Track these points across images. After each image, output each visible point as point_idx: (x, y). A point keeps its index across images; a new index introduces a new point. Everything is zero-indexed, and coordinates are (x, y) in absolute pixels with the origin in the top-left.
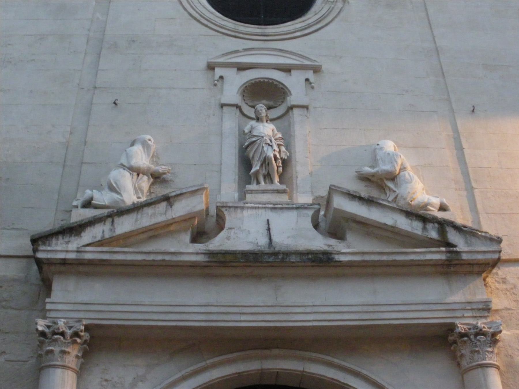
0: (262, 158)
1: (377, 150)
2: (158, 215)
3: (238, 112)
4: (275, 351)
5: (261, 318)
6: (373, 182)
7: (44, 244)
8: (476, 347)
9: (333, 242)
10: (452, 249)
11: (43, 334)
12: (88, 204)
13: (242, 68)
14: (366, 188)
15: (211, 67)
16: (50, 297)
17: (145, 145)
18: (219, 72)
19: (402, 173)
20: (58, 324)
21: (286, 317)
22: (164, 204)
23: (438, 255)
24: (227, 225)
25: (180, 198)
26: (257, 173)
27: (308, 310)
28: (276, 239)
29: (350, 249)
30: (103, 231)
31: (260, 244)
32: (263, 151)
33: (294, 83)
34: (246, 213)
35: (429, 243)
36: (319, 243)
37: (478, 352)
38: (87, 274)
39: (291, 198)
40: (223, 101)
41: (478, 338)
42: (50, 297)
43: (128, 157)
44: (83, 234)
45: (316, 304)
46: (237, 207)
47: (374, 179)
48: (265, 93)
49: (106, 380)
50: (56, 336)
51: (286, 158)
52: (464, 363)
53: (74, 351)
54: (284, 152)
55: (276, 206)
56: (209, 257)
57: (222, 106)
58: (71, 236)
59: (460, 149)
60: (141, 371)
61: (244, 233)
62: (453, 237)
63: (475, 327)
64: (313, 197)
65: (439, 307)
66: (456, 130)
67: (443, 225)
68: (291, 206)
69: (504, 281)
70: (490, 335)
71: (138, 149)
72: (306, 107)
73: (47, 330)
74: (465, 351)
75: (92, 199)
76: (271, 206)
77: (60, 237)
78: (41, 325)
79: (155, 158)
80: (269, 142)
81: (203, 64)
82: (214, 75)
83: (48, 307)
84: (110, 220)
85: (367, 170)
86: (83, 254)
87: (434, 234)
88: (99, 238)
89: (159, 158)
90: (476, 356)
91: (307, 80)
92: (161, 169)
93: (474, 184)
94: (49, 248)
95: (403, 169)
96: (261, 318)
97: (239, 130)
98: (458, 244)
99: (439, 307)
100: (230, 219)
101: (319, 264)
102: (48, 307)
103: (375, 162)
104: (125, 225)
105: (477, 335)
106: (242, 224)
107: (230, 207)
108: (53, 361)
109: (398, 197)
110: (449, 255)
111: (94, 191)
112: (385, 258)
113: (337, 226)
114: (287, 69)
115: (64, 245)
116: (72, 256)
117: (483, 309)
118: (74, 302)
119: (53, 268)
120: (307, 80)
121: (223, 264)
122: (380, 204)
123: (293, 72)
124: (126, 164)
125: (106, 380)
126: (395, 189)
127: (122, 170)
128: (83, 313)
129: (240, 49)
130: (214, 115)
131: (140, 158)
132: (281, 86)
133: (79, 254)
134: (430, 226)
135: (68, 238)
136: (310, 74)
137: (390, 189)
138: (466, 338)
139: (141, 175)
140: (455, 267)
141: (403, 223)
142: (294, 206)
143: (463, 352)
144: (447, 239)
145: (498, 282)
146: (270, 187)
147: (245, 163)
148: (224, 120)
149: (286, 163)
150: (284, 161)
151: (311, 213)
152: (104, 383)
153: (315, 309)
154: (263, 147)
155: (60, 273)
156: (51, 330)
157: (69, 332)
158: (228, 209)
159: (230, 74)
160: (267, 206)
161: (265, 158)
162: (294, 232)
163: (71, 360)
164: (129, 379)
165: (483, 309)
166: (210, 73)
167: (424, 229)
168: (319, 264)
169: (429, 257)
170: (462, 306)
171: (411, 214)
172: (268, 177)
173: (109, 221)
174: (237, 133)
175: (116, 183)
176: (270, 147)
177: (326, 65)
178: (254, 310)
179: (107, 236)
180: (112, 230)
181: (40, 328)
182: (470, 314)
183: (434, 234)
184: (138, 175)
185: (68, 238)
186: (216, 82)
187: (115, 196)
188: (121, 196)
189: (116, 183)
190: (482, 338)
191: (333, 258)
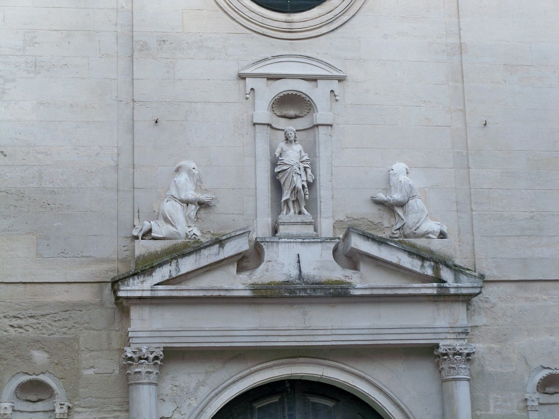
0: (292, 187)
1: (391, 176)
4: (301, 360)
5: (293, 339)
6: (386, 206)
7: (123, 284)
8: (454, 364)
9: (349, 272)
10: (442, 284)
11: (131, 359)
12: (147, 234)
14: (379, 212)
15: (242, 77)
16: (130, 327)
17: (190, 173)
19: (410, 201)
20: (142, 351)
21: (311, 338)
22: (217, 246)
23: (431, 289)
24: (266, 258)
25: (230, 240)
26: (287, 202)
27: (328, 332)
28: (305, 271)
29: (363, 281)
30: (170, 271)
31: (292, 276)
32: (292, 181)
33: (318, 94)
34: (281, 246)
35: (425, 279)
36: (337, 273)
37: (454, 368)
38: (157, 305)
39: (315, 230)
40: (255, 121)
41: (456, 357)
42: (130, 327)
44: (154, 274)
45: (334, 328)
46: (273, 242)
47: (387, 204)
48: (292, 104)
49: (176, 386)
50: (142, 361)
51: (311, 181)
54: (310, 175)
55: (305, 241)
56: (254, 293)
57: (254, 124)
58: (144, 276)
60: (202, 378)
61: (279, 264)
62: (446, 274)
64: (334, 221)
65: (428, 331)
67: (439, 261)
68: (316, 240)
70: (465, 355)
71: (183, 178)
73: (134, 356)
75: (150, 231)
76: (301, 240)
77: (136, 277)
79: (199, 184)
80: (298, 171)
82: (245, 86)
83: (130, 335)
84: (175, 261)
85: (382, 196)
86: (156, 292)
87: (429, 272)
88: (167, 278)
89: (202, 183)
90: (452, 371)
92: (204, 197)
94: (128, 288)
96: (293, 339)
97: (271, 154)
98: (448, 281)
99: (428, 331)
100: (269, 253)
101: (337, 295)
102: (130, 335)
103: (388, 186)
104: (187, 265)
105: (455, 354)
106: (278, 257)
107: (268, 242)
108: (141, 380)
109: (405, 226)
110: (439, 290)
111: (152, 223)
112: (389, 292)
113: (353, 260)
114: (313, 79)
115: (140, 285)
116: (147, 294)
117: (463, 333)
118: (150, 329)
119: (131, 302)
122: (388, 245)
123: (318, 81)
125: (176, 386)
126: (403, 217)
128: (158, 338)
129: (269, 56)
130: (247, 134)
132: (307, 99)
133: (153, 292)
134: (427, 264)
135: (142, 278)
136: (334, 85)
138: (446, 357)
139: (190, 205)
141: (406, 261)
142: (319, 240)
143: (443, 366)
144: (440, 276)
146: (300, 218)
147: (277, 186)
148: (256, 141)
149: (311, 185)
150: (309, 184)
151: (332, 246)
152: (175, 388)
153: (334, 332)
154: (293, 176)
155: (136, 304)
156: (138, 355)
157: (151, 356)
158: (266, 243)
159: (259, 84)
160: (297, 240)
161: (295, 187)
162: (318, 263)
164: (193, 385)
165: (463, 333)
166: (242, 82)
167: (422, 266)
169: (423, 291)
170: (447, 330)
173: (174, 262)
174: (269, 154)
176: (299, 176)
177: (350, 71)
178: (288, 333)
179: (174, 275)
180: (178, 270)
181: (129, 355)
182: (453, 336)
183: (429, 272)
184: (187, 205)
185: (142, 278)
186: (248, 96)
188: (176, 229)
191: (349, 293)
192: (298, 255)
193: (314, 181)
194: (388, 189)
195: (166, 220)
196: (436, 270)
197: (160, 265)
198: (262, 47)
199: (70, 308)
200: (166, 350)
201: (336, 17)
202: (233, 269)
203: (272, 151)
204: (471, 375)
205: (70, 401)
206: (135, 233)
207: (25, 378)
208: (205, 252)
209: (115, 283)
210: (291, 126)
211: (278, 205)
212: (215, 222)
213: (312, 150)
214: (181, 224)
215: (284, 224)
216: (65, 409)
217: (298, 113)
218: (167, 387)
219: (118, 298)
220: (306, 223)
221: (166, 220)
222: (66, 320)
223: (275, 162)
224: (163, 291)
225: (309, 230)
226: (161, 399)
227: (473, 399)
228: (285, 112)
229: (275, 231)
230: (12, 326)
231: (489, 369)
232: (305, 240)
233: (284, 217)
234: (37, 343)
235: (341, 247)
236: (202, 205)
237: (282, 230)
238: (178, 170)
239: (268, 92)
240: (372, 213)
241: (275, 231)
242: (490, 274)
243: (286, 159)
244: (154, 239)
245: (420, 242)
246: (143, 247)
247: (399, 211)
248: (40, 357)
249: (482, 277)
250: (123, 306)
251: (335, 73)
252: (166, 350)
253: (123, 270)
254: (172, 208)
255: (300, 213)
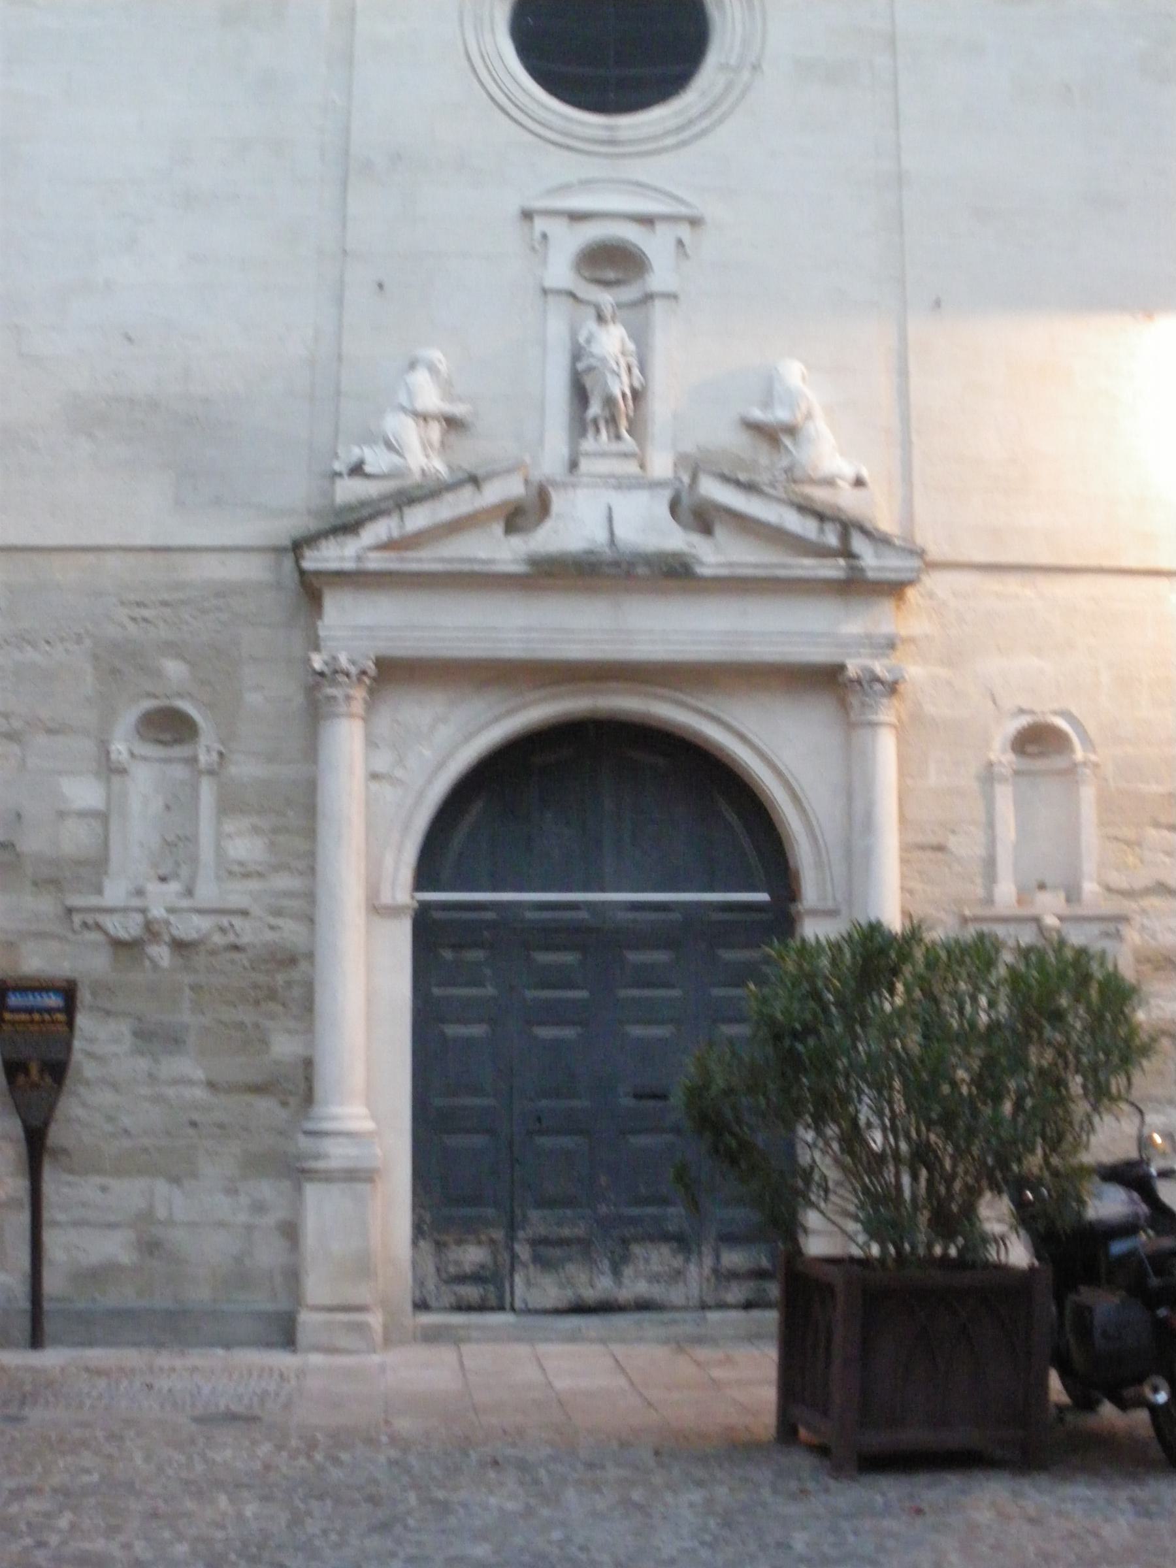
2: (462, 503)
3: (571, 300)
11: (322, 674)
12: (357, 470)
13: (576, 217)
15: (527, 215)
17: (432, 369)
18: (540, 224)
23: (833, 569)
26: (595, 422)
28: (621, 533)
33: (656, 246)
35: (821, 551)
36: (675, 539)
39: (642, 466)
40: (548, 284)
43: (410, 393)
48: (612, 262)
52: (854, 717)
53: (359, 693)
57: (545, 292)
59: (903, 373)
62: (859, 544)
63: (872, 672)
66: (903, 339)
67: (848, 526)
69: (931, 595)
71: (421, 379)
72: (672, 297)
74: (854, 701)
78: (318, 662)
79: (447, 389)
80: (615, 367)
81: (513, 207)
82: (532, 228)
85: (757, 414)
87: (832, 539)
91: (680, 243)
92: (458, 409)
93: (914, 438)
95: (809, 416)
100: (558, 502)
101: (674, 575)
104: (418, 518)
113: (702, 518)
114: (647, 221)
116: (349, 566)
118: (355, 627)
120: (680, 243)
121: (549, 575)
124: (405, 403)
127: (403, 417)
131: (430, 398)
136: (684, 231)
137: (786, 447)
140: (855, 586)
141: (794, 522)
145: (922, 596)
146: (615, 447)
147: (580, 394)
149: (637, 395)
159: (557, 229)
162: (643, 524)
163: (358, 707)
167: (821, 531)
168: (674, 575)
171: (805, 508)
172: (612, 421)
175: (397, 440)
179: (396, 534)
183: (832, 539)
187: (396, 459)
189: (397, 440)
190: (878, 687)
192: (610, 509)
193: (645, 387)
194: (767, 403)
195: (389, 446)
196: (845, 536)
197: (372, 517)
198: (561, 167)
199: (224, 591)
200: (380, 662)
201: (691, 122)
202: (498, 529)
203: (574, 334)
204: (900, 720)
205: (222, 743)
206: (338, 466)
207: (147, 704)
208: (449, 497)
209: (298, 547)
210: (606, 298)
211: (580, 425)
212: (470, 453)
213: (640, 336)
214: (420, 455)
215: (587, 454)
216: (215, 756)
217: (620, 275)
218: (384, 721)
219: (302, 573)
220: (625, 455)
221: (389, 446)
222: (219, 609)
223: (577, 354)
224: (376, 562)
225: (632, 467)
226: (371, 743)
227: (902, 760)
228: (599, 274)
229: (573, 465)
230: (134, 619)
231: (929, 709)
232: (622, 484)
233: (588, 444)
234: (173, 649)
235: (685, 500)
236: (452, 423)
237: (585, 465)
238: (413, 365)
239: (568, 242)
240: (737, 442)
241: (573, 465)
242: (935, 552)
243: (595, 349)
244: (368, 476)
245: (820, 495)
246: (349, 490)
247: (787, 441)
248: (174, 668)
249: (920, 553)
250: (311, 590)
251: (683, 210)
252: (380, 662)
253: (313, 525)
254: (408, 432)
255: (618, 437)
